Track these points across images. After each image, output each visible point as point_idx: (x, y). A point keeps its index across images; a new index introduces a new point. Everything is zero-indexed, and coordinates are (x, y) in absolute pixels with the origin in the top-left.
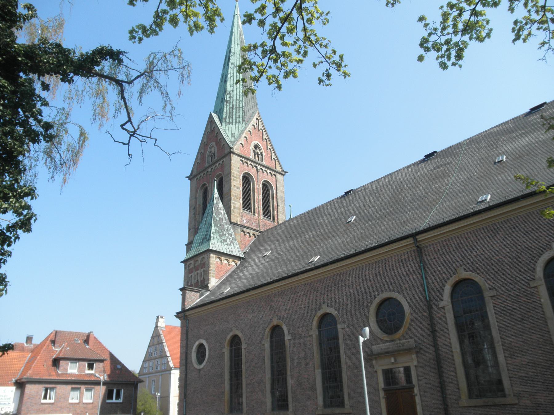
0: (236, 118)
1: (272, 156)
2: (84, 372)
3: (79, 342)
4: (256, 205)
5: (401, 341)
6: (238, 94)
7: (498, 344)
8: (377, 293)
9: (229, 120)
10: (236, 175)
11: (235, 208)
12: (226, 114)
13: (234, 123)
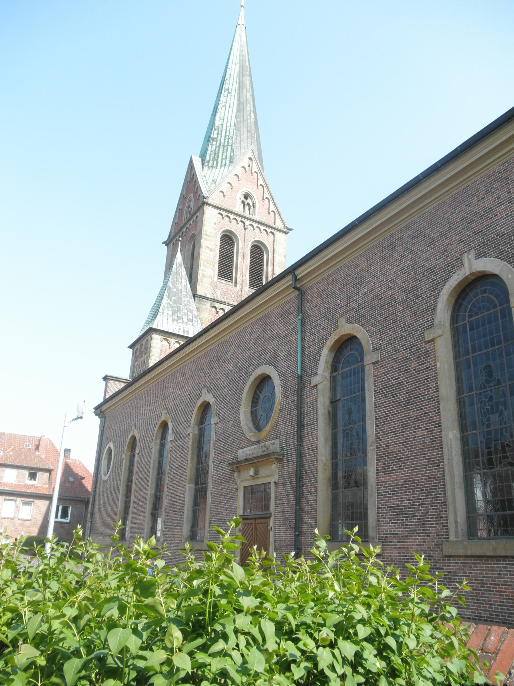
1: (270, 208)
2: (24, 482)
3: (30, 447)
4: (239, 273)
6: (228, 128)
7: (371, 448)
9: (213, 163)
11: (204, 276)
12: (210, 156)
13: (219, 167)
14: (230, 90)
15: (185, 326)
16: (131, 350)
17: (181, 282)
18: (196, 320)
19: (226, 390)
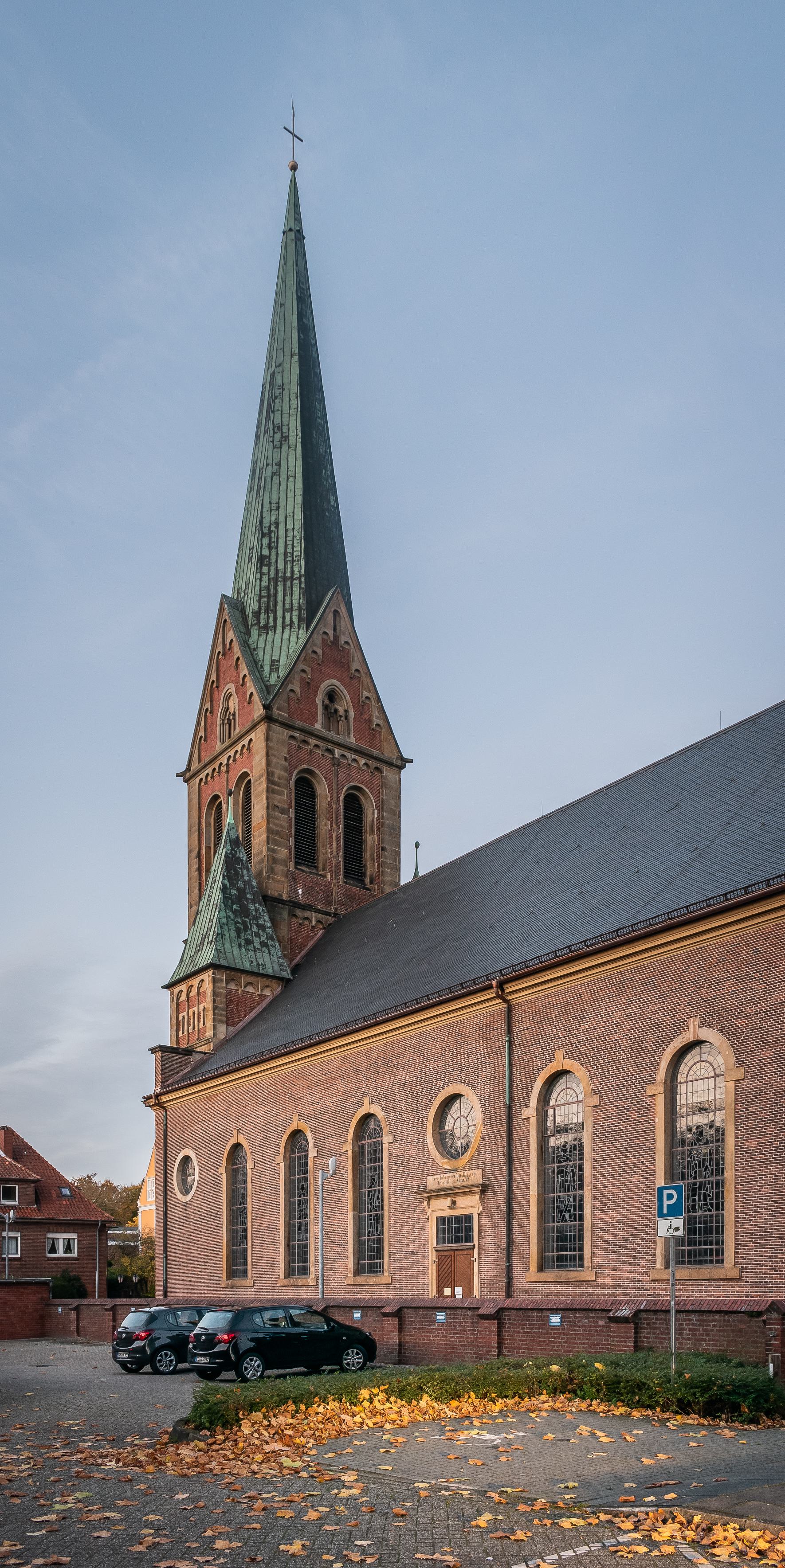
0: (284, 611)
5: (466, 1172)
8: (442, 1084)
9: (268, 618)
10: (279, 778)
13: (279, 629)
14: (285, 429)
15: (258, 955)
16: (167, 992)
17: (243, 876)
18: (273, 943)
19: (402, 1104)
